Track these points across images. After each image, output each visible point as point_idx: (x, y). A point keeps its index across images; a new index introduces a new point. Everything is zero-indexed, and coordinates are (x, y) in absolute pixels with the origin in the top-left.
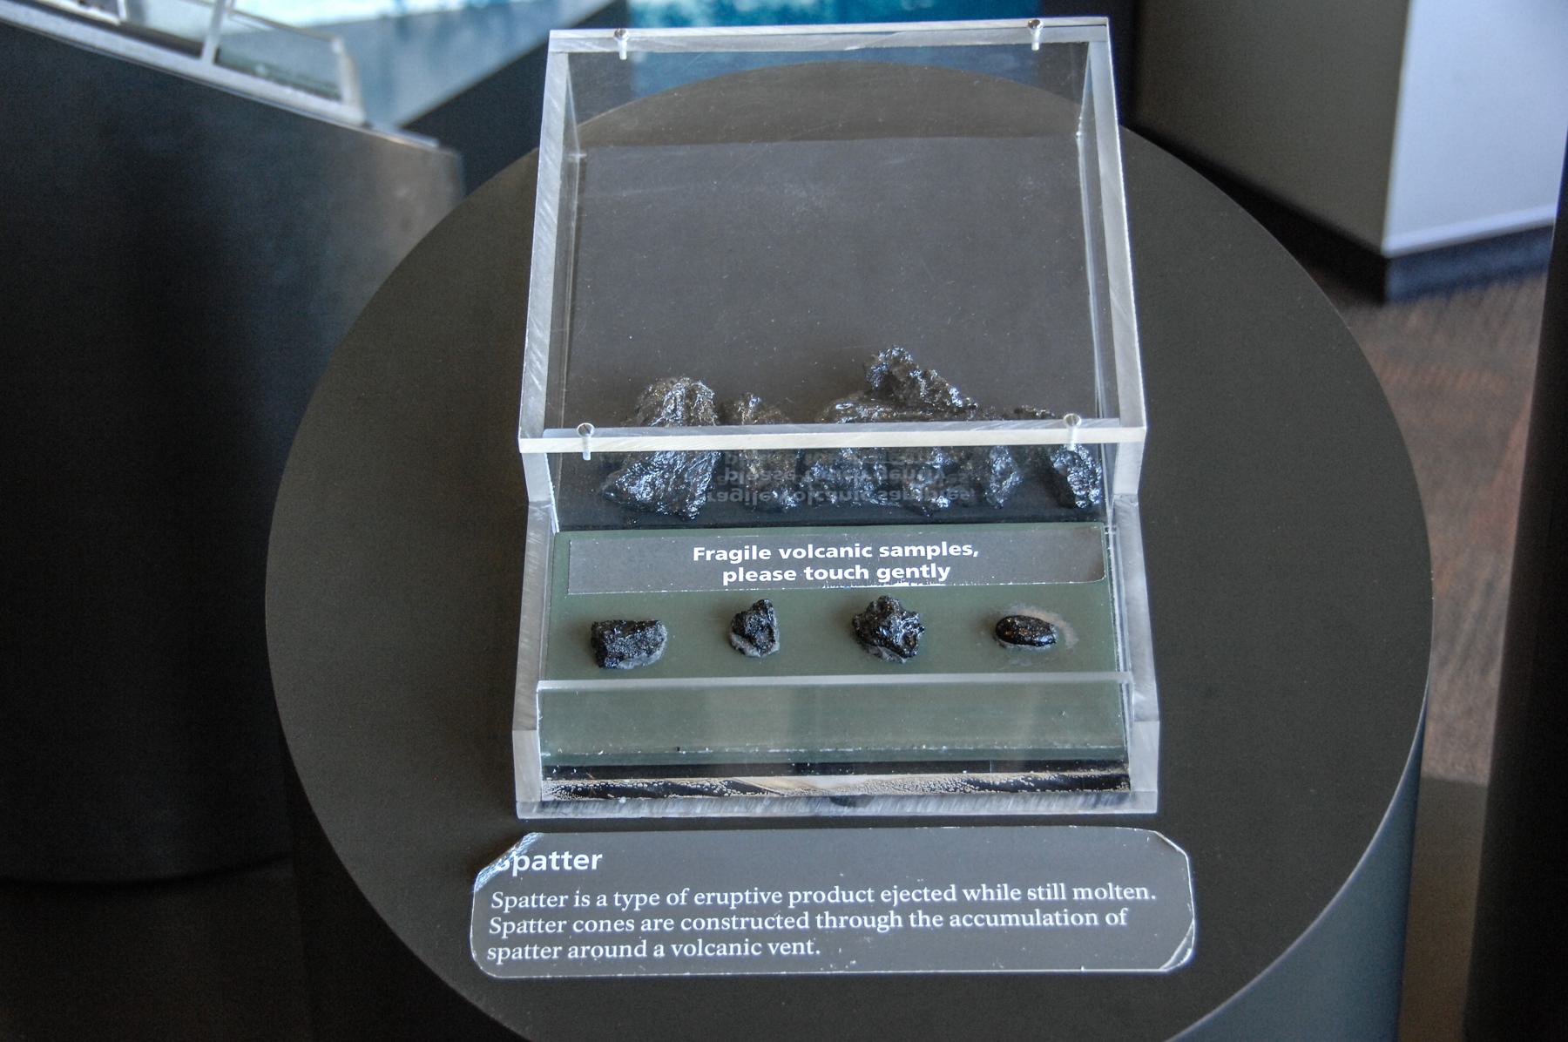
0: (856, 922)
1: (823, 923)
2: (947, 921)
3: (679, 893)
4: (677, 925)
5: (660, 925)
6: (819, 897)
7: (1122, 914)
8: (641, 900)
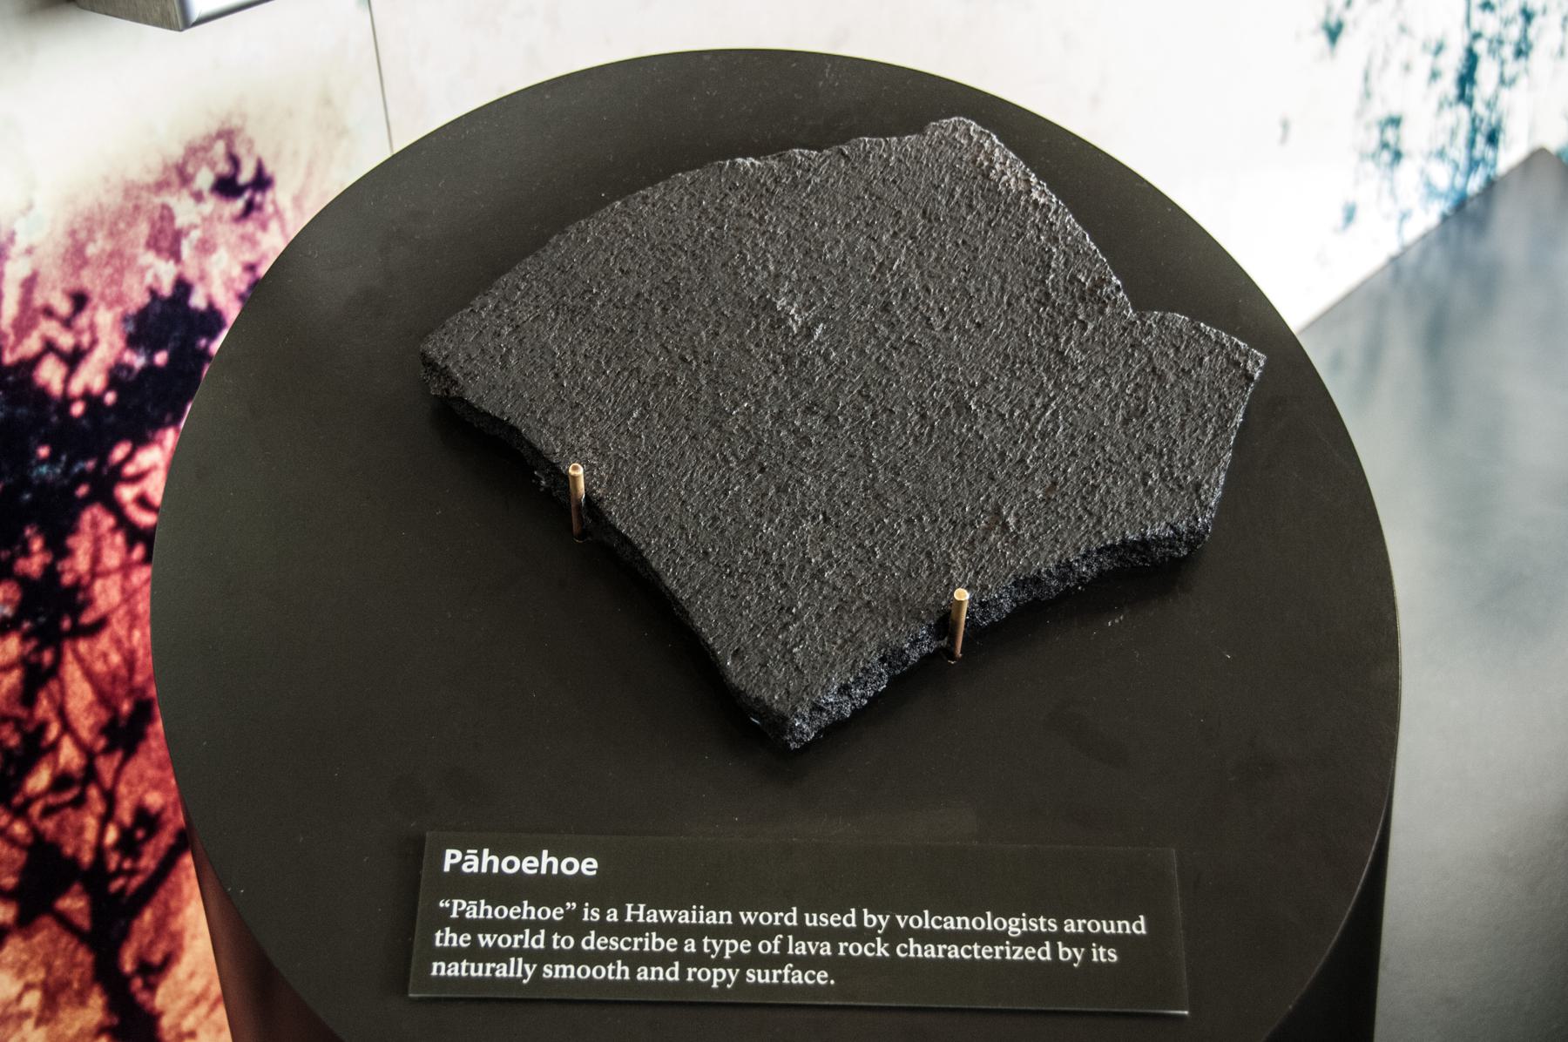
0: (1094, 927)
2: (681, 945)
3: (771, 940)
4: (754, 947)
6: (856, 949)
7: (776, 942)
8: (732, 947)
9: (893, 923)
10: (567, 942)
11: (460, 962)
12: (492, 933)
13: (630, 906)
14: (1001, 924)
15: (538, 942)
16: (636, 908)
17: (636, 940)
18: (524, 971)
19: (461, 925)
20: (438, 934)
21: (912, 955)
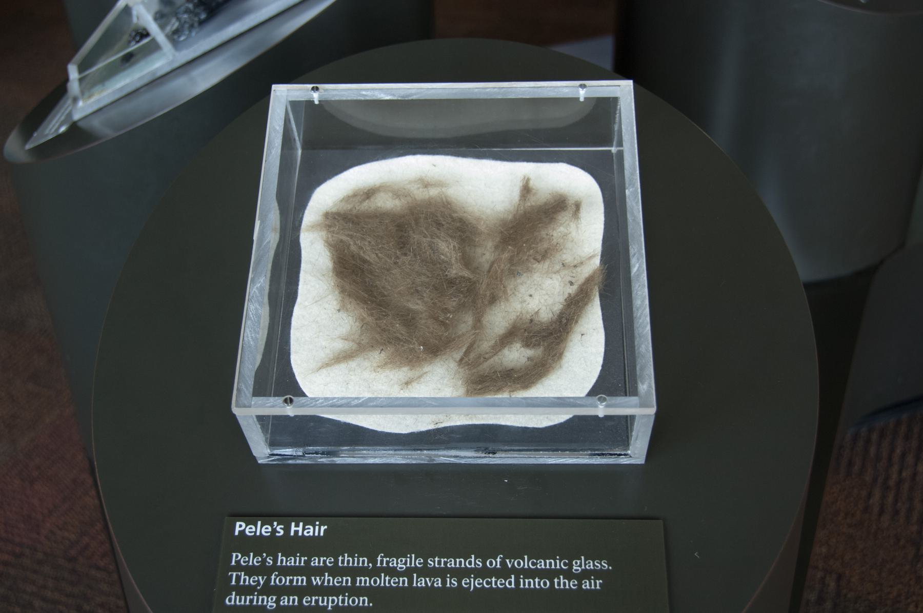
1: (559, 584)
2: (580, 584)
5: (325, 562)
7: (498, 560)
10: (545, 584)
13: (293, 524)
16: (297, 525)
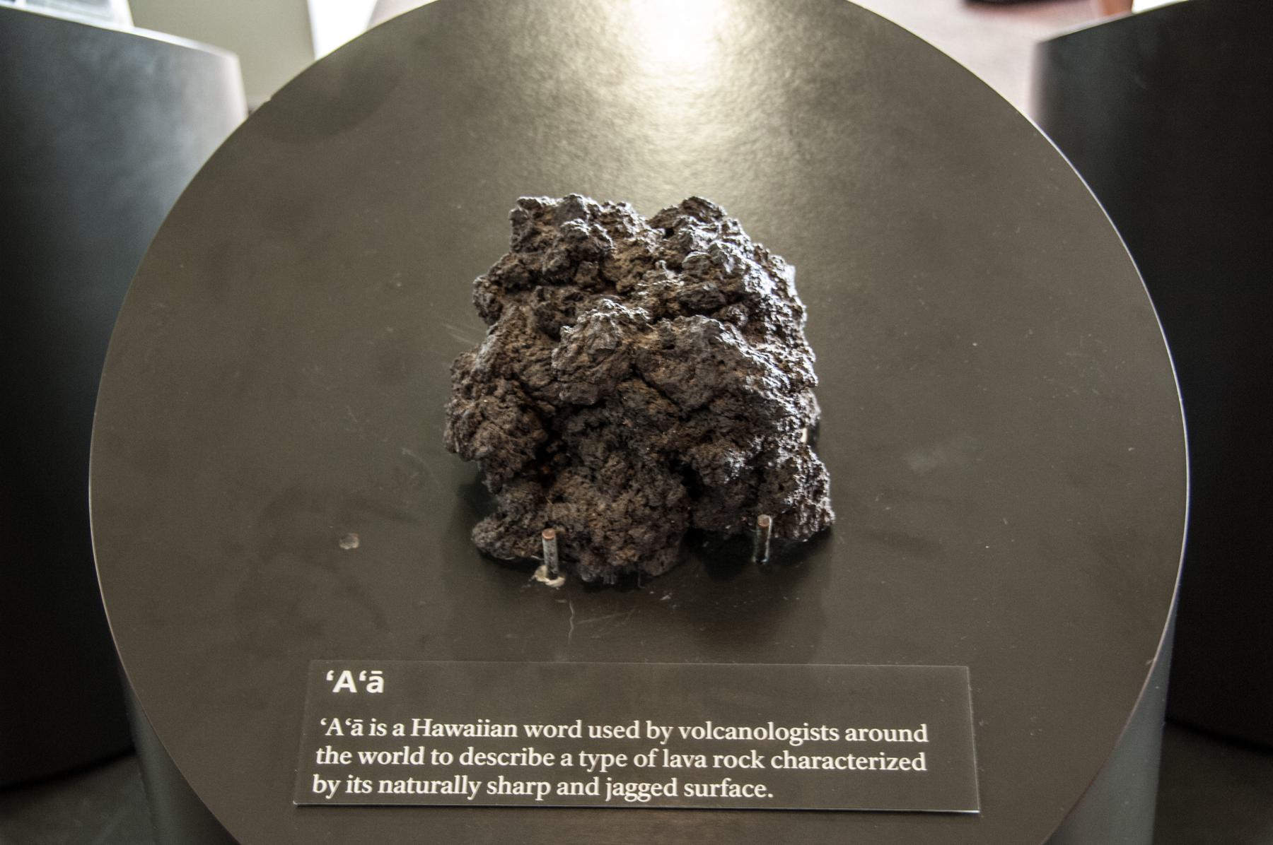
0: (876, 735)
2: (558, 759)
3: (647, 754)
4: (630, 761)
7: (652, 755)
8: (608, 760)
9: (675, 735)
10: (446, 759)
11: (406, 780)
12: (372, 750)
13: (416, 721)
14: (782, 734)
15: (417, 758)
16: (422, 723)
17: (514, 756)
18: (468, 786)
19: (341, 744)
20: (320, 752)
21: (787, 766)
